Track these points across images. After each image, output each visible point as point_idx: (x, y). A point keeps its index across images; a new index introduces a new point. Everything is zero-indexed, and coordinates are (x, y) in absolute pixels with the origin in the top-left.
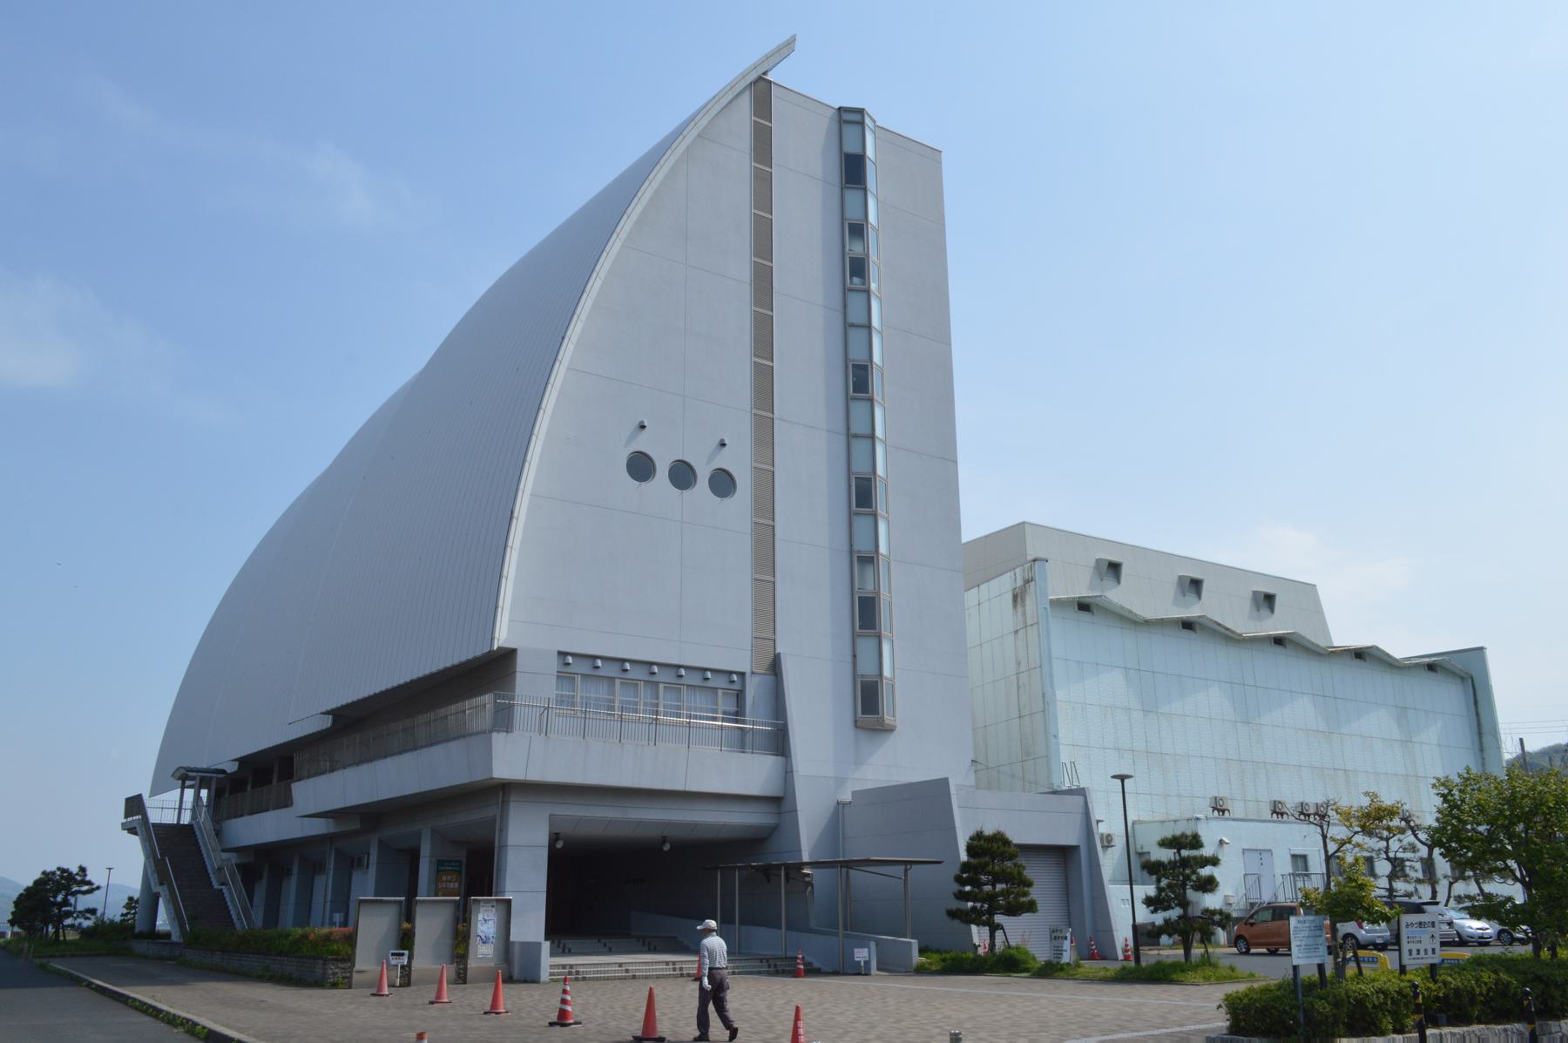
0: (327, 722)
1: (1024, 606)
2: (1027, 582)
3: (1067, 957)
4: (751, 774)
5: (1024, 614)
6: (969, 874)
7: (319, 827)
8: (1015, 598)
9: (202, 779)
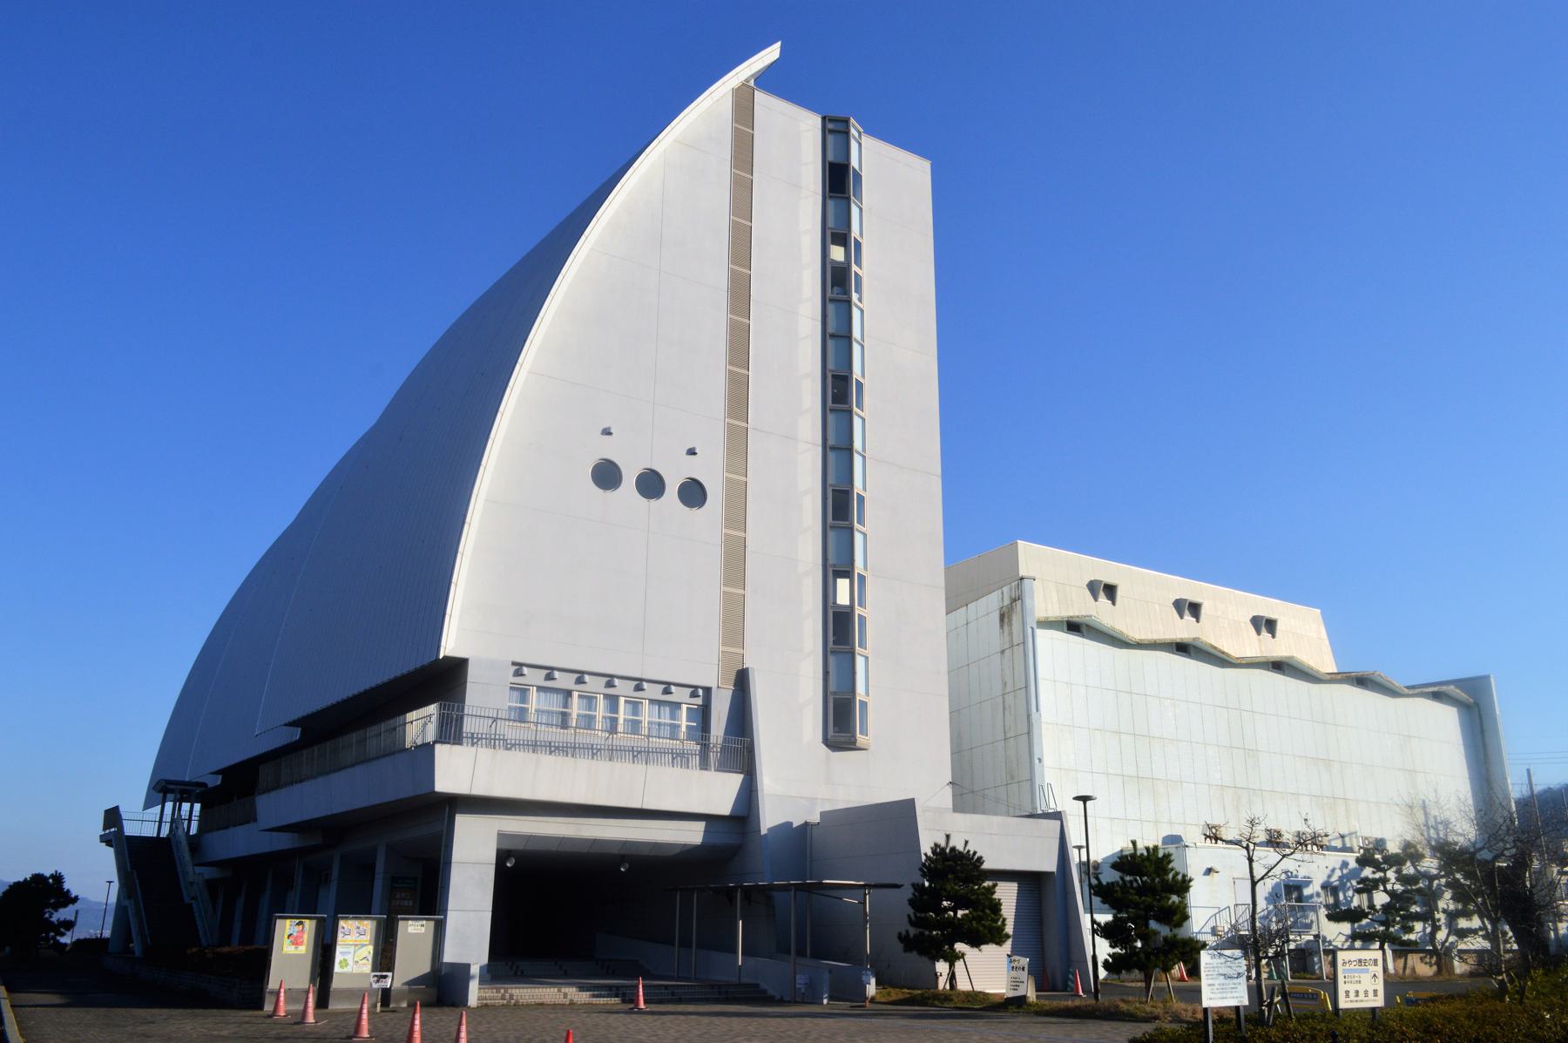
0: (296, 734)
1: (1010, 621)
2: (1014, 600)
3: (334, 1006)
4: (717, 793)
5: (1011, 634)
6: (923, 901)
7: (284, 842)
8: (1002, 617)
9: (182, 792)
